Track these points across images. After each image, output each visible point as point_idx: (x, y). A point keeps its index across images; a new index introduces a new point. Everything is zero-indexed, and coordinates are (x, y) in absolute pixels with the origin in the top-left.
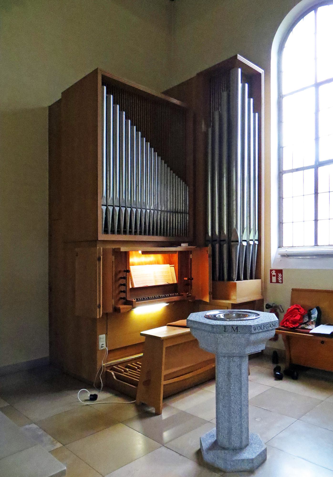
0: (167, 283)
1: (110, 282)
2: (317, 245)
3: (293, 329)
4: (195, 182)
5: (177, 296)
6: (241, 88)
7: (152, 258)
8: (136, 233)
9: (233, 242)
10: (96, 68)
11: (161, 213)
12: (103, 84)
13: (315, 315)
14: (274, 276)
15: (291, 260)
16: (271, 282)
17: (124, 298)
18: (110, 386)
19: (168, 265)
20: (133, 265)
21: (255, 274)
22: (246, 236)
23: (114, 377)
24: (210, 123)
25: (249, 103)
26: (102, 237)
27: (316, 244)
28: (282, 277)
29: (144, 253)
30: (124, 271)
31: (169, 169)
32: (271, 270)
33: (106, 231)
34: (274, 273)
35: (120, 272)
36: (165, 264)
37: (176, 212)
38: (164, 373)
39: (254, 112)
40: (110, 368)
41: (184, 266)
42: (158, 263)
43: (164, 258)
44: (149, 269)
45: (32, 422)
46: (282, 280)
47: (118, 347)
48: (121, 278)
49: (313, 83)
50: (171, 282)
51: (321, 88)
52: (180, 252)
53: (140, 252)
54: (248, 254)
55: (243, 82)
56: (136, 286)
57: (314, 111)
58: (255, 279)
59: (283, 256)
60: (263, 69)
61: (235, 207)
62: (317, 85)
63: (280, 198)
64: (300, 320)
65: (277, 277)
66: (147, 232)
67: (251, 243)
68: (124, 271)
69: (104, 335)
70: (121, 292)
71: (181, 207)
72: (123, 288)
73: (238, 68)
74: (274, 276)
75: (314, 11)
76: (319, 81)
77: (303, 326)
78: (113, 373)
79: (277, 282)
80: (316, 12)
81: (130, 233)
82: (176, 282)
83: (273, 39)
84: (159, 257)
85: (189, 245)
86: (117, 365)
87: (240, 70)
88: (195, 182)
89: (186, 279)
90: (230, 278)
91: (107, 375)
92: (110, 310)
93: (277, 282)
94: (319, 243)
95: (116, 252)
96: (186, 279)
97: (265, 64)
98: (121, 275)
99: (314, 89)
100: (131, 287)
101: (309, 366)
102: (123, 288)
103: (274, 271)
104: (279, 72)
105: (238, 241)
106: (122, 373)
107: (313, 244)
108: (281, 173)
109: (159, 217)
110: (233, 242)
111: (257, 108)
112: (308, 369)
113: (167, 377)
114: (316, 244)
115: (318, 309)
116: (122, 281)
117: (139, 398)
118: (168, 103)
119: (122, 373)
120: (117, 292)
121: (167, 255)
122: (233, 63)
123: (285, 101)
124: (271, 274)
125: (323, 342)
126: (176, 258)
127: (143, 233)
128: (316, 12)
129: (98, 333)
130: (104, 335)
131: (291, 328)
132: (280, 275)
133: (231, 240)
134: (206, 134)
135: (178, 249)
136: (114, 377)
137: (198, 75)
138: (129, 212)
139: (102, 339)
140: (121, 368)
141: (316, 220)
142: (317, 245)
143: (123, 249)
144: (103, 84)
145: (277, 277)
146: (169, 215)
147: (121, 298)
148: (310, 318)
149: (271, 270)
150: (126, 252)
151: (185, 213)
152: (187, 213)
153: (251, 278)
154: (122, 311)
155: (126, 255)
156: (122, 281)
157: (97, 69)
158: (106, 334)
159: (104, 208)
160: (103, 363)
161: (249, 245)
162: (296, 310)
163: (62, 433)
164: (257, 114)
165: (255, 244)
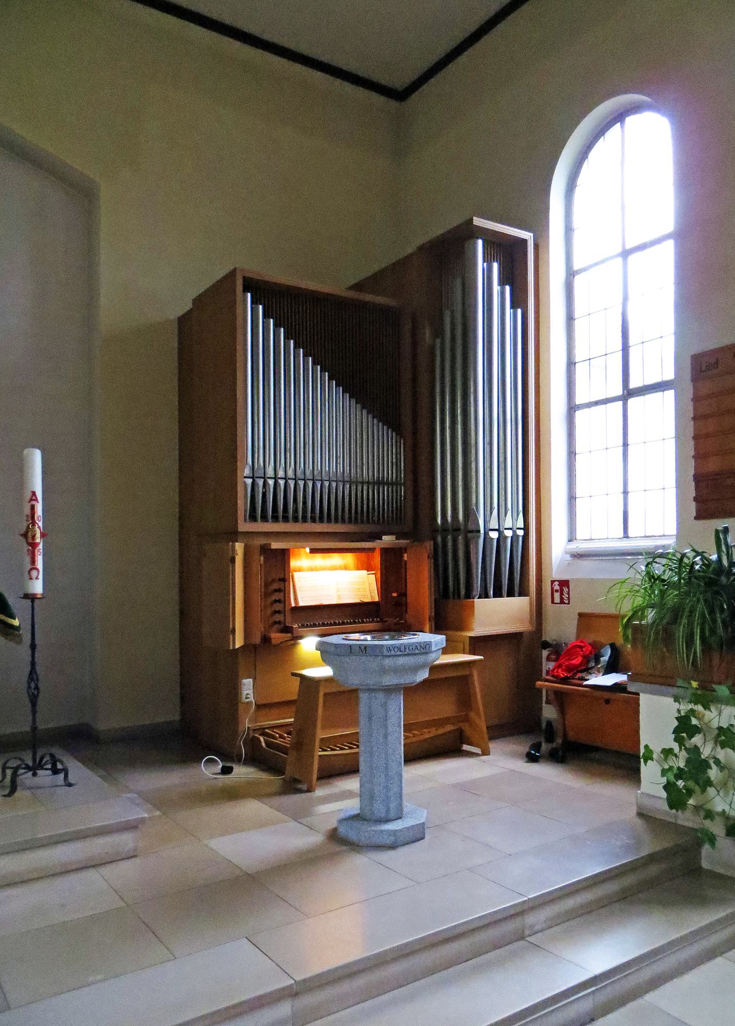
0: (359, 601)
1: (257, 598)
2: (628, 537)
3: (564, 681)
4: (415, 434)
5: (377, 622)
6: (484, 270)
7: (336, 559)
8: (305, 519)
9: (470, 532)
10: (232, 268)
11: (350, 487)
12: (246, 289)
13: (605, 659)
14: (557, 591)
15: (585, 564)
16: (553, 602)
17: (279, 622)
18: (256, 758)
19: (365, 572)
20: (299, 570)
21: (513, 586)
22: (497, 520)
23: (263, 744)
24: (438, 333)
25: (500, 293)
26: (244, 526)
27: (626, 536)
28: (568, 594)
29: (313, 551)
30: (280, 580)
31: (365, 412)
32: (553, 582)
33: (253, 518)
34: (557, 587)
35: (273, 580)
36: (358, 569)
37: (380, 483)
38: (321, 734)
39: (514, 306)
40: (260, 732)
41: (392, 572)
42: (346, 568)
43: (358, 559)
44: (328, 577)
45: (131, 791)
46: (569, 598)
47: (276, 700)
48: (276, 591)
49: (620, 250)
50: (368, 599)
51: (632, 258)
52: (385, 552)
53: (308, 550)
54: (488, 553)
55: (487, 259)
56: (301, 603)
57: (621, 301)
58: (519, 596)
59: (579, 556)
60: (529, 231)
61: (474, 474)
62: (626, 254)
63: (572, 453)
64: (580, 665)
65: (562, 594)
66: (333, 518)
67: (509, 533)
68: (280, 580)
69: (251, 680)
70: (276, 612)
71: (389, 474)
72: (278, 607)
73: (477, 238)
74: (557, 591)
75: (619, 124)
76: (628, 247)
77: (580, 675)
78: (262, 739)
79: (562, 602)
80: (622, 127)
81: (296, 519)
82: (377, 599)
83: (552, 174)
84: (349, 558)
85: (397, 539)
86: (272, 728)
87: (480, 242)
88: (415, 434)
89: (395, 595)
90: (469, 595)
91: (252, 743)
92: (257, 640)
93: (562, 602)
94: (630, 534)
95: (265, 550)
96: (395, 595)
97: (537, 220)
98: (275, 586)
99: (620, 259)
100: (293, 605)
101: (600, 745)
102: (278, 607)
103: (557, 583)
104: (569, 230)
105: (479, 531)
106: (275, 738)
107: (622, 535)
108: (572, 408)
109: (347, 492)
110: (470, 532)
111: (519, 301)
112: (596, 749)
113: (326, 743)
114: (626, 536)
115: (613, 646)
116: (276, 596)
117: (289, 771)
118: (364, 305)
119: (275, 738)
120: (269, 611)
121: (363, 555)
122: (467, 232)
123: (579, 282)
124: (552, 589)
125: (607, 701)
126: (377, 559)
127: (326, 520)
128: (622, 127)
129: (240, 674)
130: (251, 680)
131: (562, 679)
132: (565, 590)
133: (467, 530)
134: (432, 349)
135: (377, 544)
136: (263, 744)
137: (421, 248)
138: (292, 486)
139: (247, 687)
140: (276, 733)
141: (625, 493)
142: (628, 537)
143: (275, 545)
144: (246, 289)
145: (562, 594)
146: (365, 488)
147: (275, 623)
148: (597, 661)
149: (553, 582)
150: (284, 550)
151: (396, 483)
152: (401, 485)
153: (511, 594)
154: (274, 642)
155: (283, 556)
156: (276, 596)
157: (235, 269)
158: (255, 679)
159: (249, 481)
160: (247, 723)
161: (501, 539)
162: (578, 649)
163: (163, 802)
164: (519, 311)
165: (515, 537)
